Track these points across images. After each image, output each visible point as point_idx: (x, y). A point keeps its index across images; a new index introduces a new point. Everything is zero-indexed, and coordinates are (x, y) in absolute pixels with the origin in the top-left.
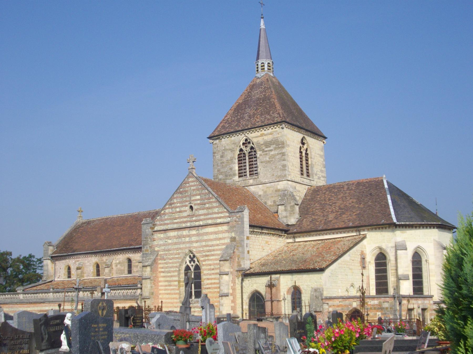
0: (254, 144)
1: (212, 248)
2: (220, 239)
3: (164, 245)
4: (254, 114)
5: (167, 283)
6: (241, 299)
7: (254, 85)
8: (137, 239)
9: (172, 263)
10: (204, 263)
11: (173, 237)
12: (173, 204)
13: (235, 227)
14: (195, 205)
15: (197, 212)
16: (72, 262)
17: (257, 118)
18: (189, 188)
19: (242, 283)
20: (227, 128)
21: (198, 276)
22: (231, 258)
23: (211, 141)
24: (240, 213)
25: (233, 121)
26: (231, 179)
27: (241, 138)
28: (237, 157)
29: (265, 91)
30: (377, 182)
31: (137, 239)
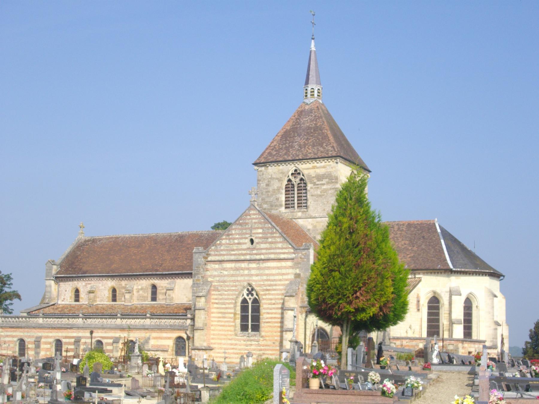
0: (305, 175)
1: (274, 283)
2: (283, 274)
3: (218, 276)
4: (305, 145)
5: (220, 315)
6: (303, 335)
7: (302, 112)
8: (162, 264)
9: (228, 295)
10: (264, 297)
11: (229, 268)
12: (231, 235)
13: (300, 263)
14: (256, 238)
15: (258, 245)
16: (82, 285)
17: (309, 149)
18: (250, 221)
19: (305, 319)
20: (274, 156)
21: (256, 309)
22: (296, 294)
23: (256, 168)
24: (306, 251)
25: (281, 149)
26: (277, 209)
27: (290, 168)
28: (284, 187)
29: (316, 121)
30: (429, 225)
31: (162, 264)
